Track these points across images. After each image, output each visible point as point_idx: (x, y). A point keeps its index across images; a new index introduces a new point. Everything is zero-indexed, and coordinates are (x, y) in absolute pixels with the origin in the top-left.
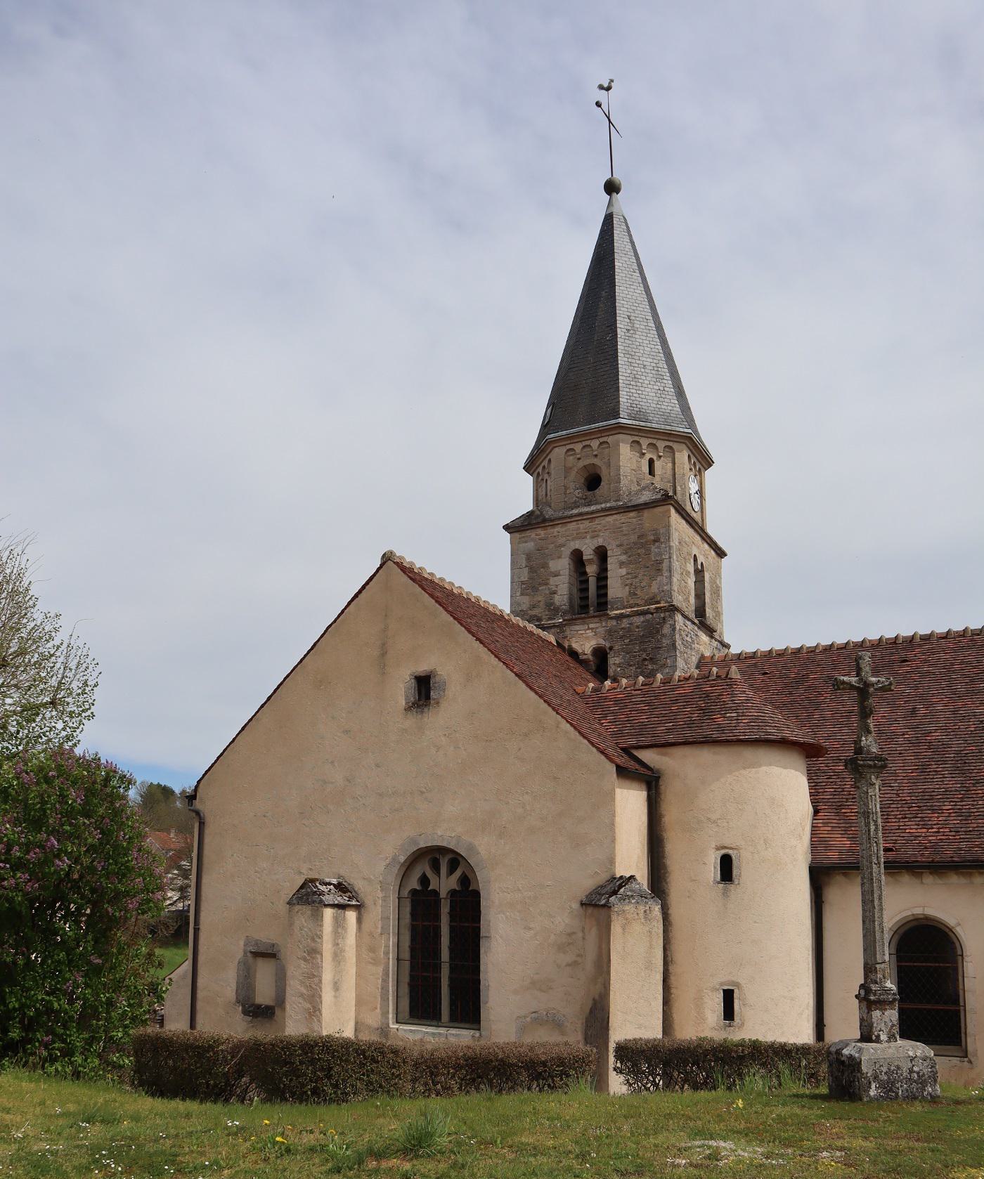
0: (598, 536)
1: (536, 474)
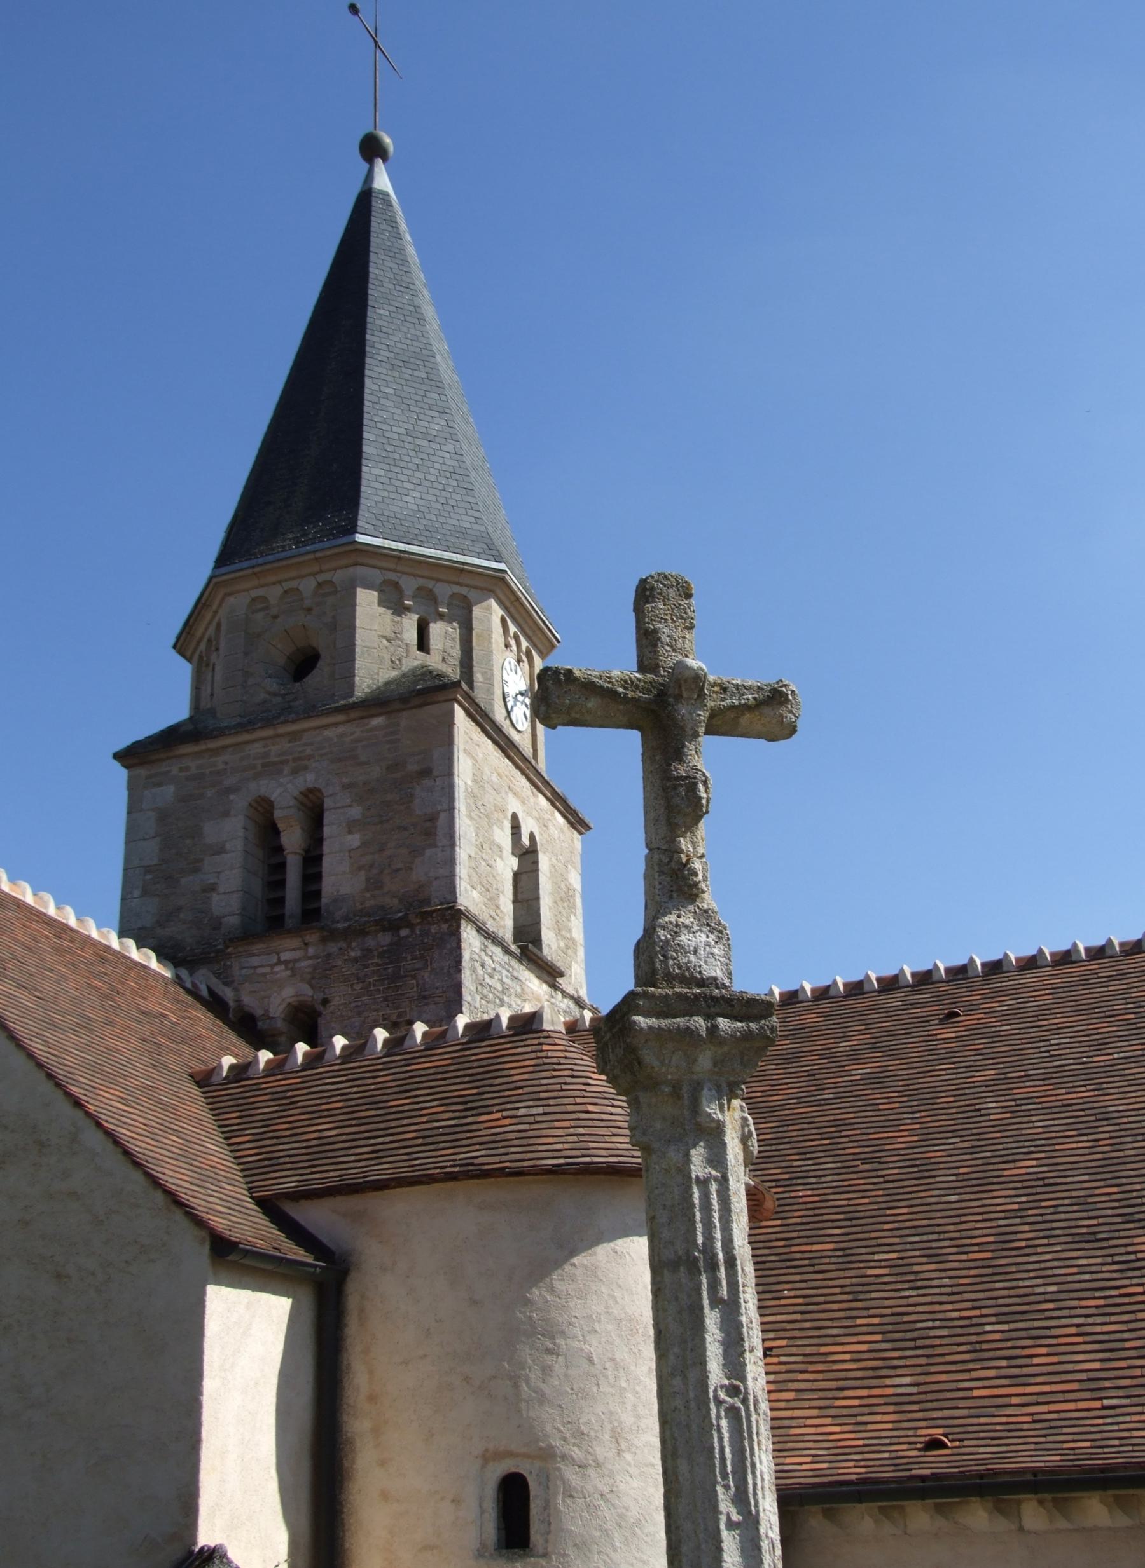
0: (306, 768)
1: (196, 657)
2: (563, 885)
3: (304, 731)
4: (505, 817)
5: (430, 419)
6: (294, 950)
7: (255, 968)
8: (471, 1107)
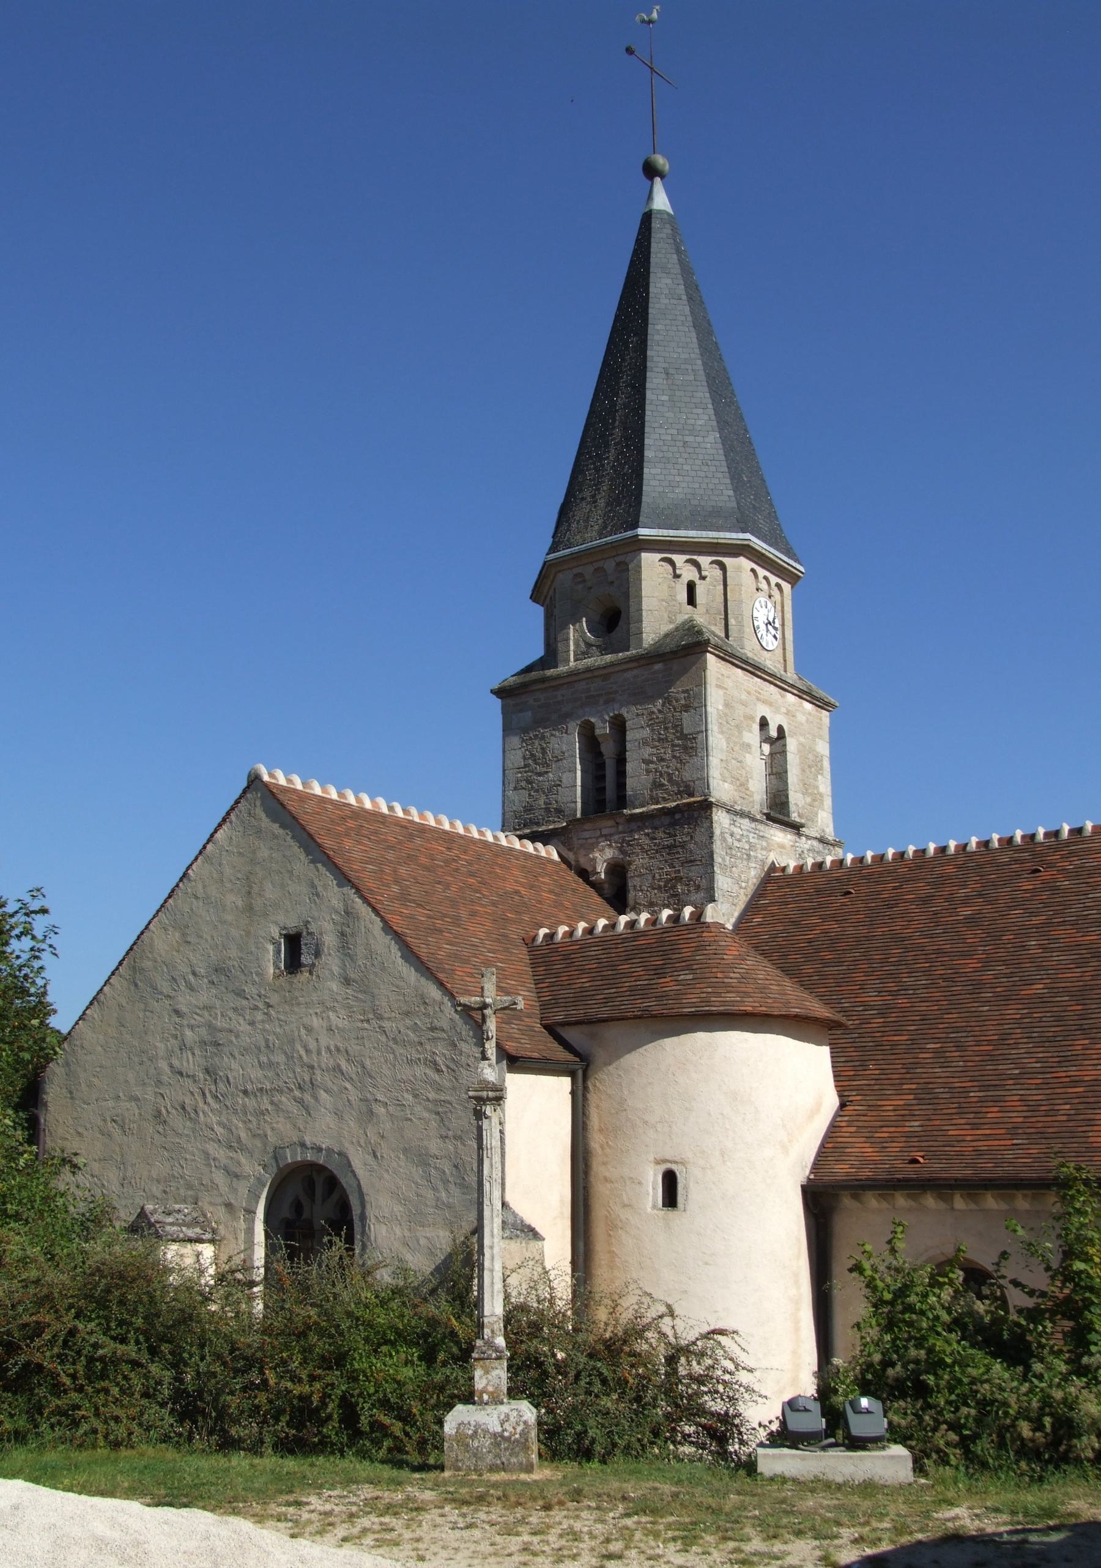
0: (613, 700)
2: (810, 756)
3: (612, 673)
4: (754, 722)
5: (696, 417)
6: (611, 827)
7: (586, 839)
8: (659, 972)
